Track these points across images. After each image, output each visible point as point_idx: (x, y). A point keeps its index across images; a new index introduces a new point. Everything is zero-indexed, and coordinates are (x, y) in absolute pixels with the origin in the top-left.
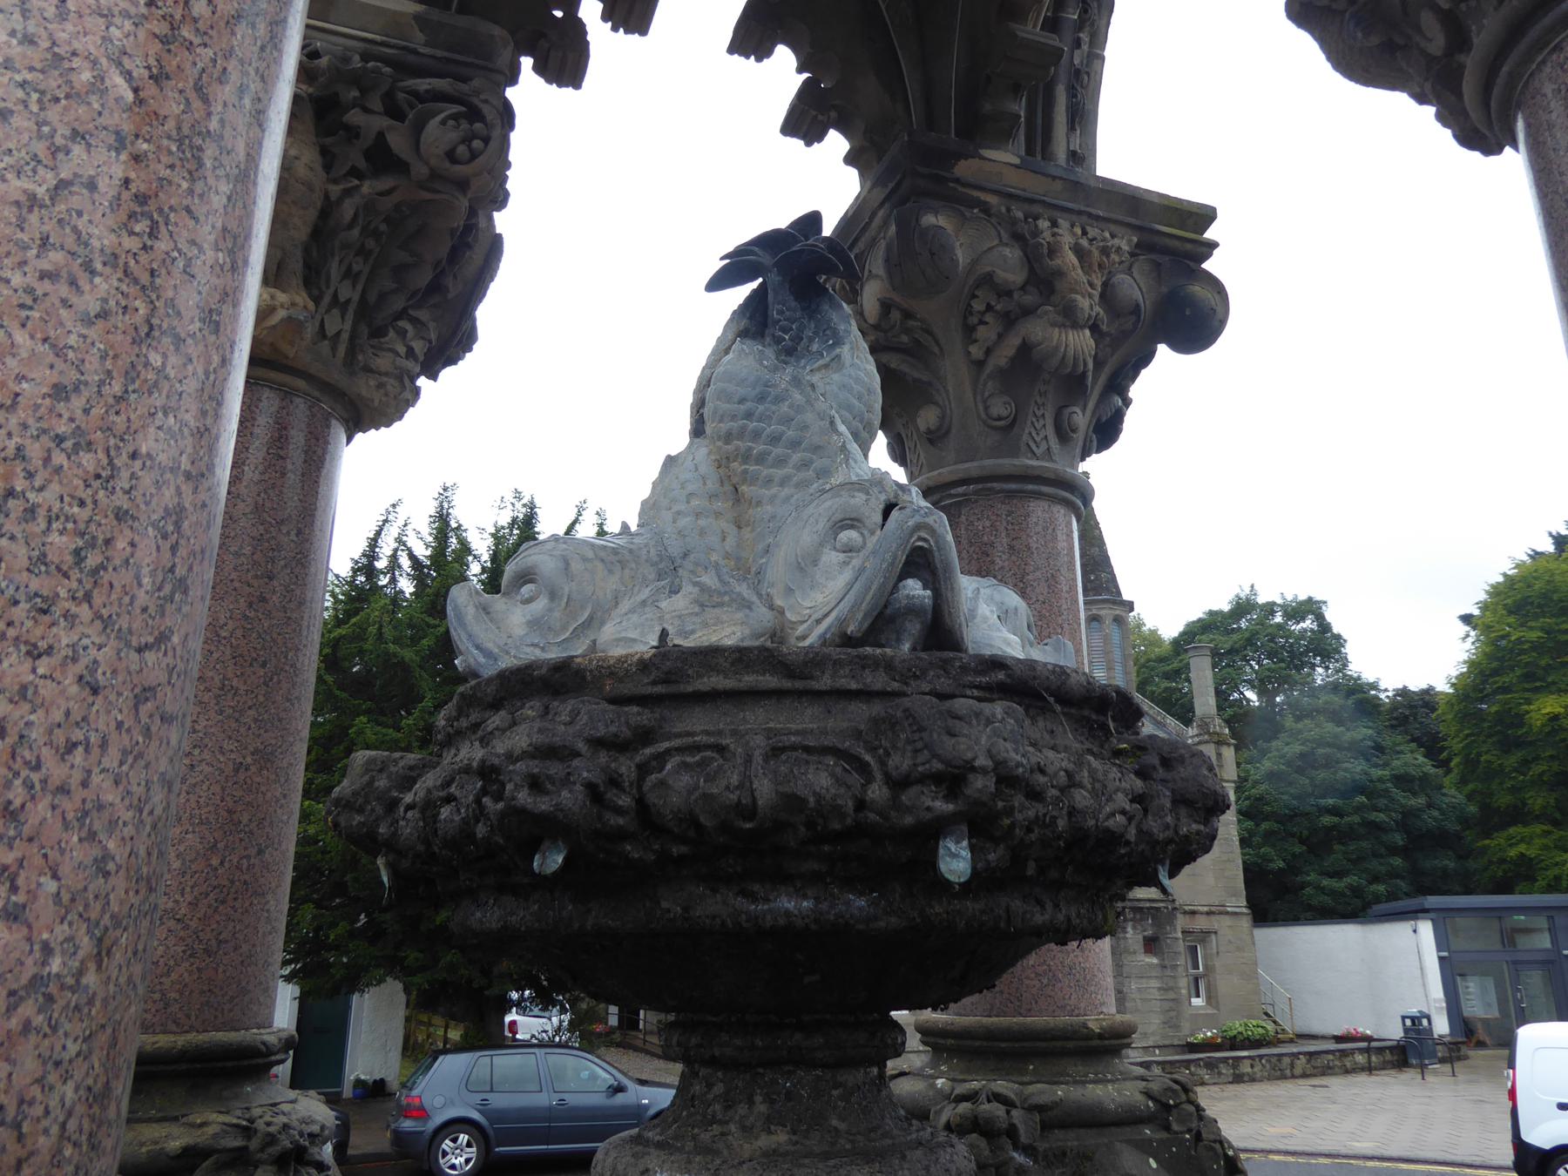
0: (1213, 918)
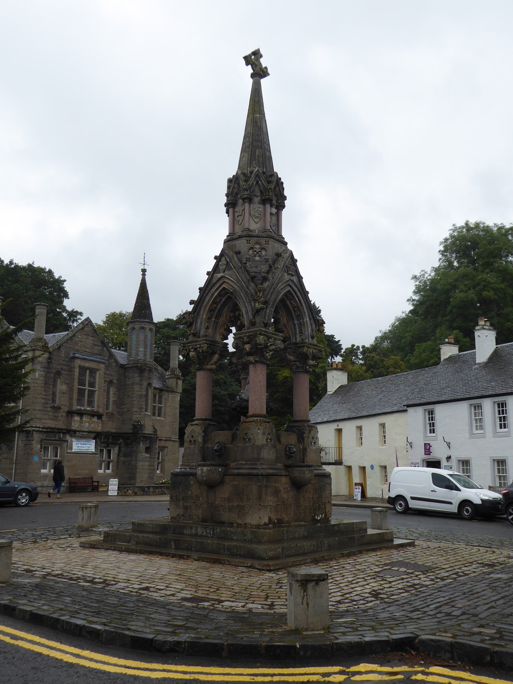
0: (167, 442)
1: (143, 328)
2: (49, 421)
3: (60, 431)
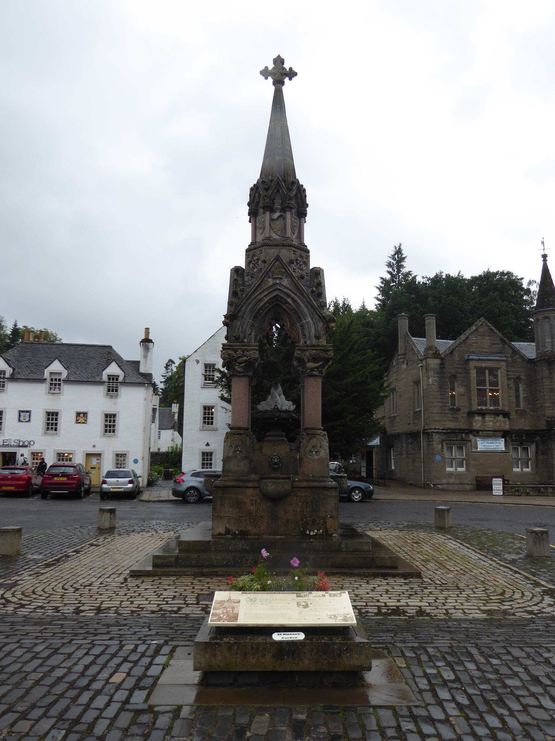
1: (547, 317)
2: (449, 423)
3: (461, 431)
